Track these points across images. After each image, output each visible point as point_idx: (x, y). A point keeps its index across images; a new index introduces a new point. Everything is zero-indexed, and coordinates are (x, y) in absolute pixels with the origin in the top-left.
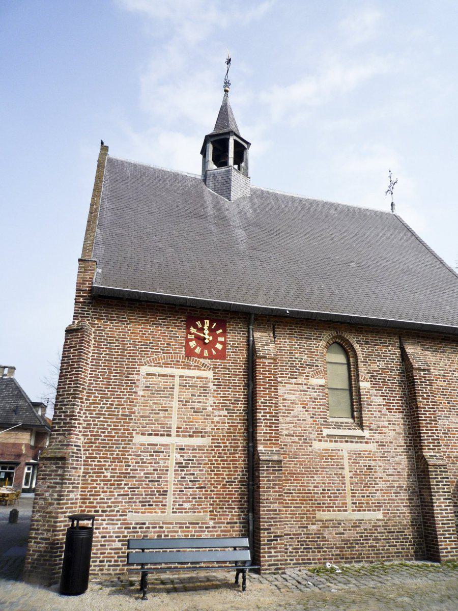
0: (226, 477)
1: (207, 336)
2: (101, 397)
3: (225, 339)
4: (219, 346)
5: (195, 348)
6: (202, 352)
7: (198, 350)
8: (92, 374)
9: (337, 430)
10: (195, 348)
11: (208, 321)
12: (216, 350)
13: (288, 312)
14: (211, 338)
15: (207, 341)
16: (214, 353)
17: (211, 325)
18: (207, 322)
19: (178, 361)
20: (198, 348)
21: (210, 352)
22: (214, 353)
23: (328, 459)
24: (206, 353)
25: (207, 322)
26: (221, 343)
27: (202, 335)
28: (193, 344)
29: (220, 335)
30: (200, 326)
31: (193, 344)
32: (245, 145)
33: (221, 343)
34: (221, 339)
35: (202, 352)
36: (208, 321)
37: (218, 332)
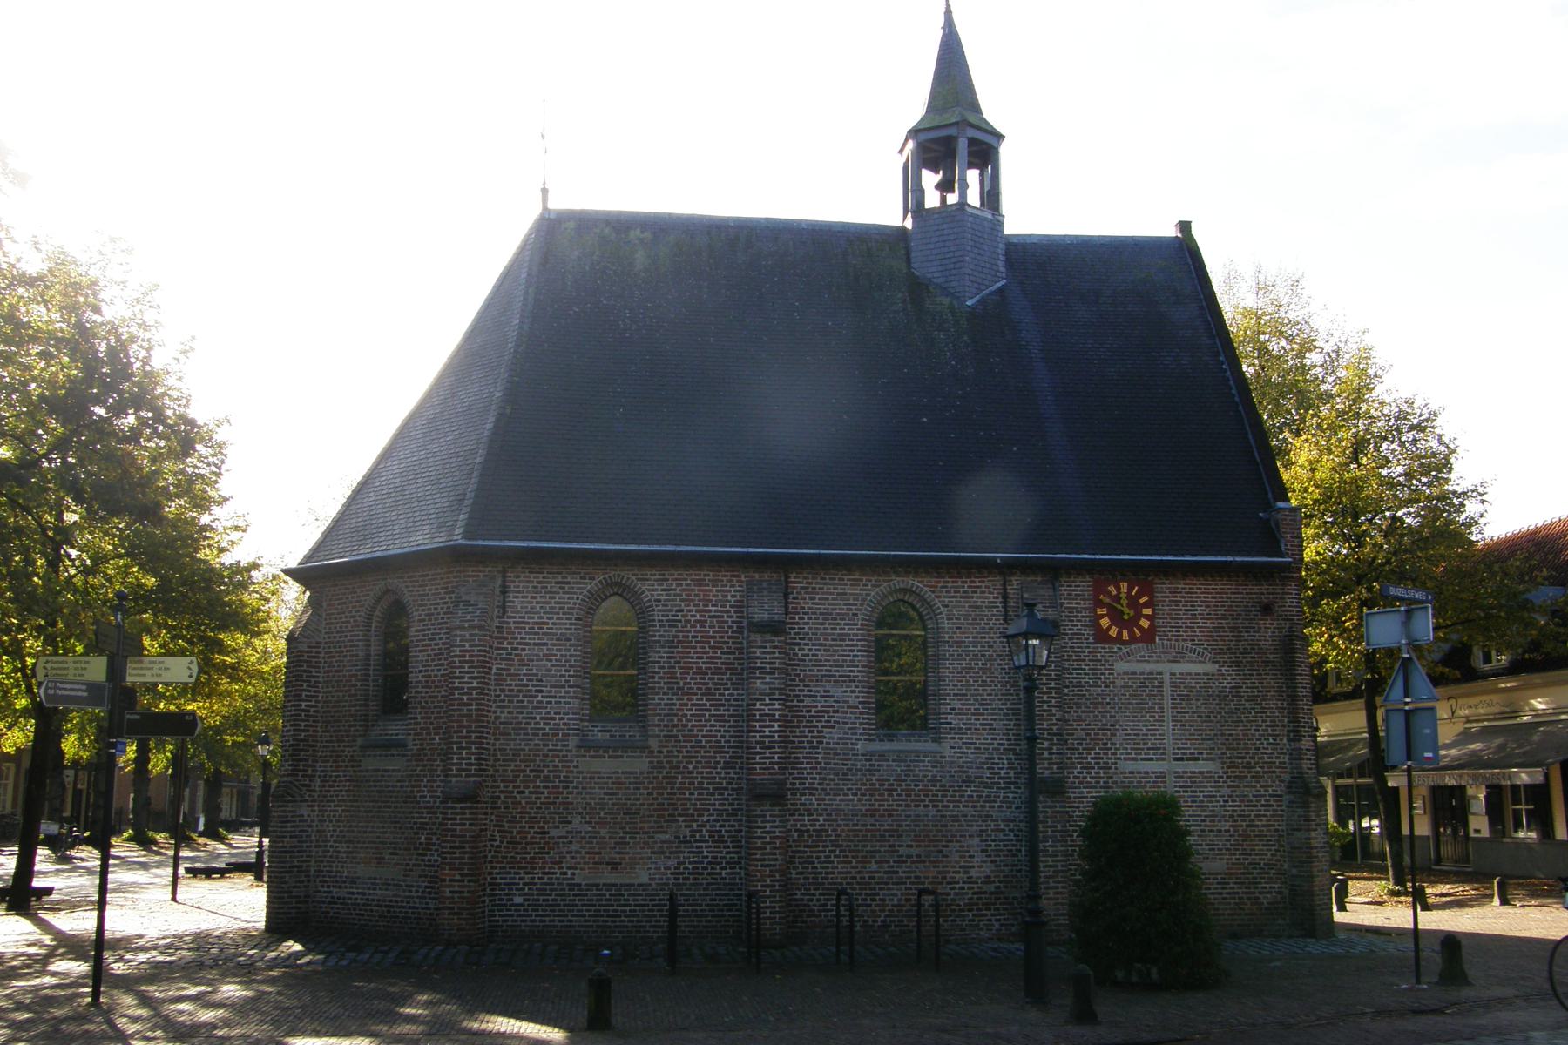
0: (729, 598)
1: (1126, 610)
2: (668, 657)
3: (1153, 612)
4: (1145, 623)
5: (1109, 628)
6: (1120, 634)
7: (1113, 632)
8: (315, 692)
9: (886, 743)
10: (1109, 628)
11: (1126, 584)
12: (1141, 628)
13: (999, 561)
14: (1132, 613)
15: (1126, 617)
16: (1138, 634)
17: (1130, 589)
18: (1124, 587)
19: (1176, 640)
20: (1114, 627)
21: (1131, 633)
22: (1138, 634)
23: (978, 899)
24: (1125, 636)
25: (1124, 587)
26: (1147, 617)
27: (1119, 607)
28: (1105, 622)
29: (1146, 605)
30: (1114, 593)
31: (1105, 622)
32: (972, 160)
33: (1147, 617)
34: (1147, 611)
35: (1120, 634)
36: (1126, 584)
37: (1142, 601)
